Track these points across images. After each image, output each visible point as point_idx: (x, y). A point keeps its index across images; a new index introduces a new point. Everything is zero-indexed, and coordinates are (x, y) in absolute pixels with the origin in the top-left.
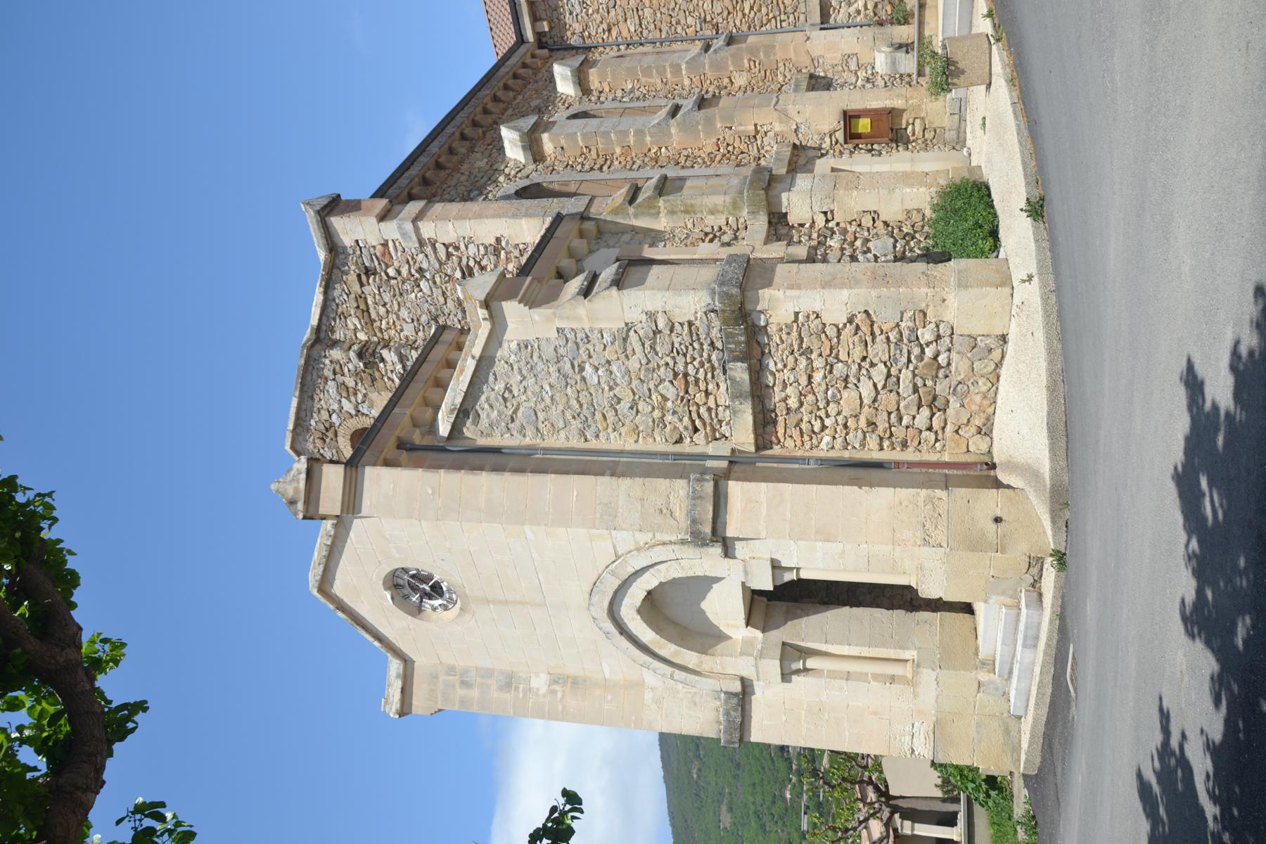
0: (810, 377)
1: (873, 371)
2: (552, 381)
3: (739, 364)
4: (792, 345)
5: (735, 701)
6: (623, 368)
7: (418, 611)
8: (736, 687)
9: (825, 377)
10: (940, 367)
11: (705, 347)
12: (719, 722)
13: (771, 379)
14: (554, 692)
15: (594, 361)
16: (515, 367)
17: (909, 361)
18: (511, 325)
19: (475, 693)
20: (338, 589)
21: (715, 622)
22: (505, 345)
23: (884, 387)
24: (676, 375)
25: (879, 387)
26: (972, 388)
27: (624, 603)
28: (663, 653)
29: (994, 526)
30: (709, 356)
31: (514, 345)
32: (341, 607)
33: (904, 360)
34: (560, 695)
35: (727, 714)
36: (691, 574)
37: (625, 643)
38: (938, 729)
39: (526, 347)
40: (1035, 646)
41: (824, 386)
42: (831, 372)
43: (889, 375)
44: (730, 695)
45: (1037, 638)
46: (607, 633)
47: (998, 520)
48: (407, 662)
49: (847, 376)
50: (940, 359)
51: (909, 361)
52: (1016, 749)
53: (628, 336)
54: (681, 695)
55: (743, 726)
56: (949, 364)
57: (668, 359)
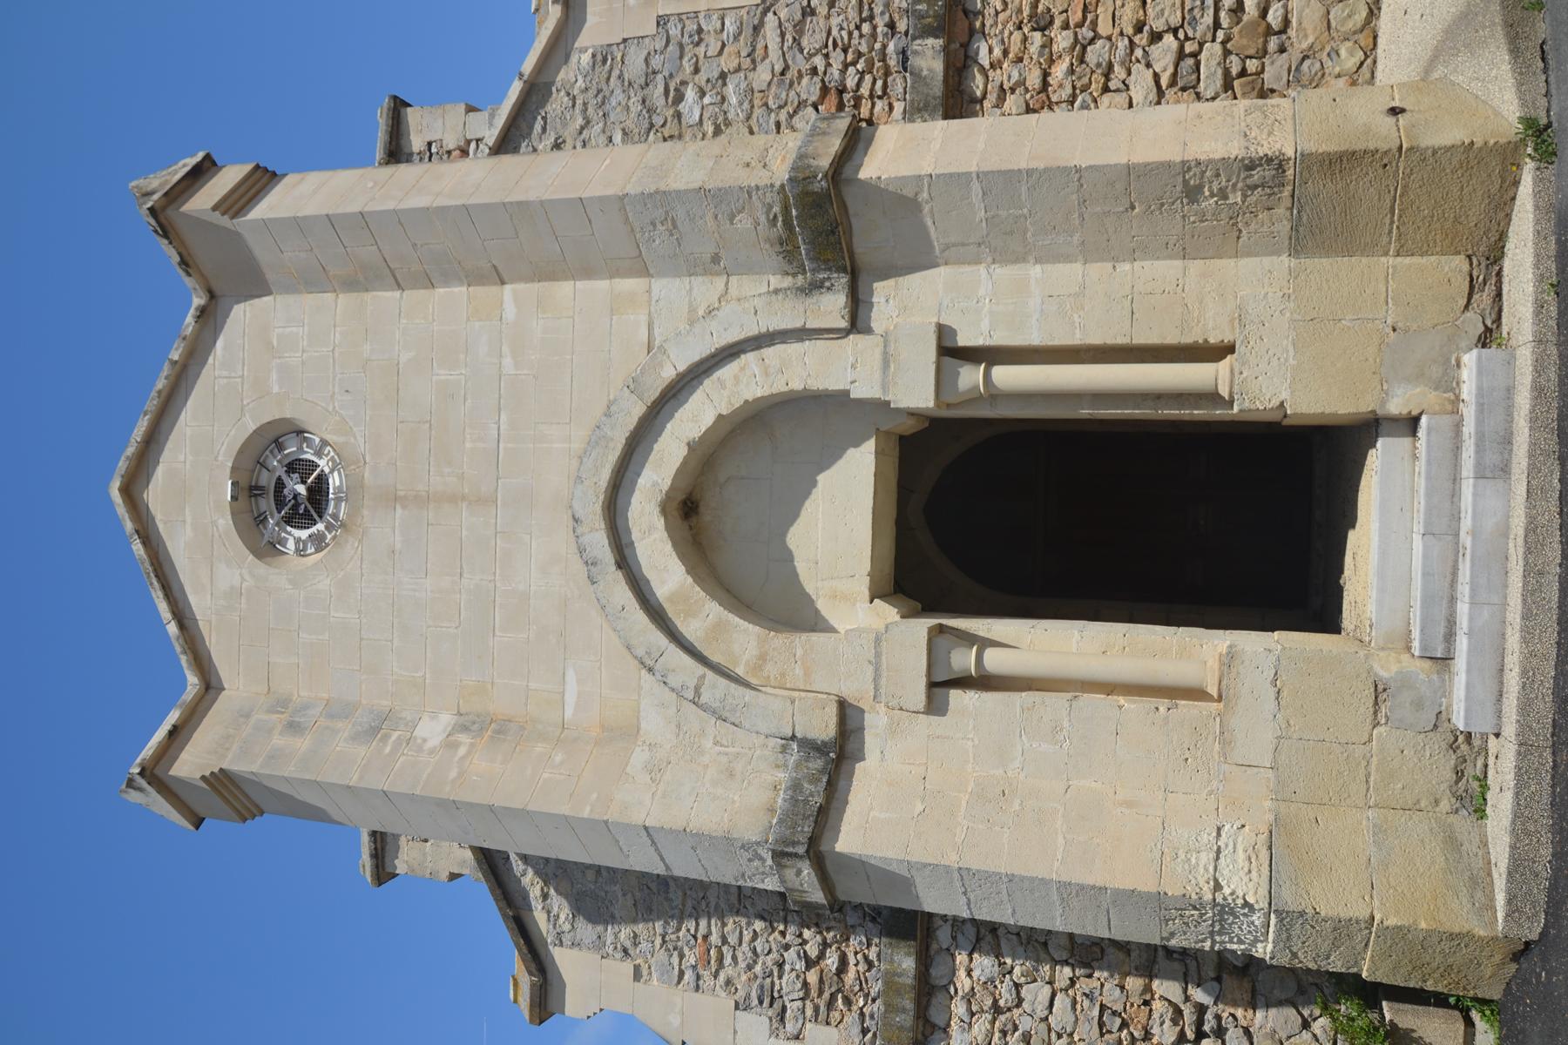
0: (1046, 75)
1: (1156, 51)
2: (629, 124)
3: (930, 41)
4: (1020, 11)
5: (817, 764)
6: (743, 85)
7: (268, 550)
8: (823, 727)
9: (1071, 71)
10: (1269, 31)
11: (879, 30)
12: (772, 810)
13: (979, 79)
14: (454, 746)
15: (701, 78)
16: (579, 102)
17: (1217, 25)
18: (591, 19)
19: (303, 744)
20: (155, 495)
21: (809, 588)
22: (574, 59)
23: (1173, 82)
24: (825, 90)
25: (1164, 82)
26: (1328, 63)
27: (641, 481)
28: (691, 629)
29: (1391, 120)
30: (884, 47)
31: (586, 58)
32: (147, 534)
33: (1208, 19)
34: (462, 751)
35: (796, 786)
36: (779, 387)
37: (623, 594)
38: (1276, 844)
39: (604, 61)
40: (1505, 470)
41: (1069, 90)
42: (1082, 61)
43: (1181, 55)
44: (811, 747)
45: (1507, 440)
46: (590, 563)
47: (1395, 111)
48: (211, 686)
49: (1110, 66)
50: (1270, 18)
51: (1217, 25)
52: (1480, 882)
53: (762, 23)
54: (706, 759)
55: (826, 815)
56: (1286, 22)
57: (819, 61)
